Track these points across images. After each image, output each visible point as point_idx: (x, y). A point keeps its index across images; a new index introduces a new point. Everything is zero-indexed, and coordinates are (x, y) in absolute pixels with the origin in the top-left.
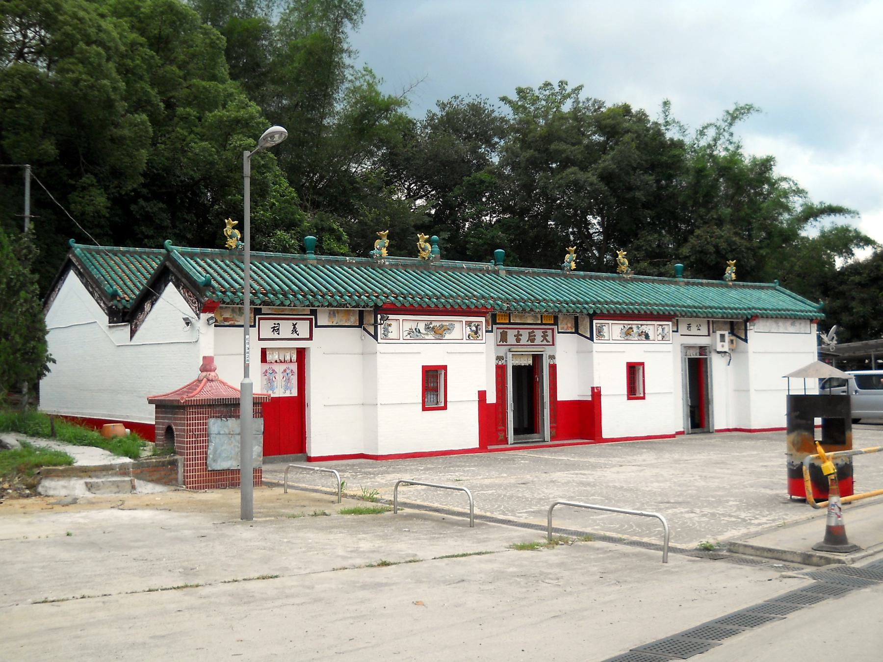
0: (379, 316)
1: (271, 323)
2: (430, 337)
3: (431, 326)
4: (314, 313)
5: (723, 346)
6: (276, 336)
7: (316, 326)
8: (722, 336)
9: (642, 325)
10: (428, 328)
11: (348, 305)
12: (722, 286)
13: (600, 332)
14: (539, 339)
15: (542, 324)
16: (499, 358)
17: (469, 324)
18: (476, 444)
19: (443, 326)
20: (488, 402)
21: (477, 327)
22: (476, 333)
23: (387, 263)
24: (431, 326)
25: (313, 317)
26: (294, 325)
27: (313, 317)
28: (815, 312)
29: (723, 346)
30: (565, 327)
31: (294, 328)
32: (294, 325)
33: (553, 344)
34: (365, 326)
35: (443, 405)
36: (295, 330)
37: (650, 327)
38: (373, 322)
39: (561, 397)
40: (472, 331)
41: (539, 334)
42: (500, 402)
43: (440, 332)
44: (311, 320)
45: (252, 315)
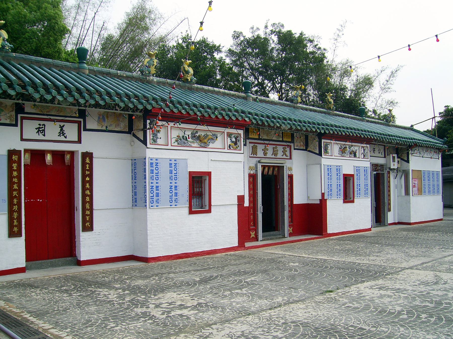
0: (148, 121)
1: (36, 124)
2: (196, 145)
3: (197, 135)
4: (82, 114)
5: (394, 165)
6: (41, 137)
7: (85, 130)
8: (394, 158)
9: (352, 146)
10: (195, 137)
11: (117, 108)
12: (279, 176)
13: (326, 150)
14: (280, 155)
15: (283, 141)
16: (250, 168)
17: (229, 135)
18: (237, 245)
19: (207, 136)
20: (245, 206)
21: (236, 139)
22: (236, 143)
23: (155, 80)
24: (197, 135)
25: (82, 120)
26: (62, 127)
27: (82, 120)
28: (442, 144)
29: (394, 165)
30: (299, 144)
31: (62, 130)
32: (62, 127)
33: (291, 158)
34: (134, 132)
35: (207, 208)
36: (62, 133)
37: (357, 147)
38: (142, 127)
39: (296, 201)
40: (232, 142)
41: (280, 149)
42: (252, 205)
43: (206, 141)
44: (79, 123)
45: (14, 113)
